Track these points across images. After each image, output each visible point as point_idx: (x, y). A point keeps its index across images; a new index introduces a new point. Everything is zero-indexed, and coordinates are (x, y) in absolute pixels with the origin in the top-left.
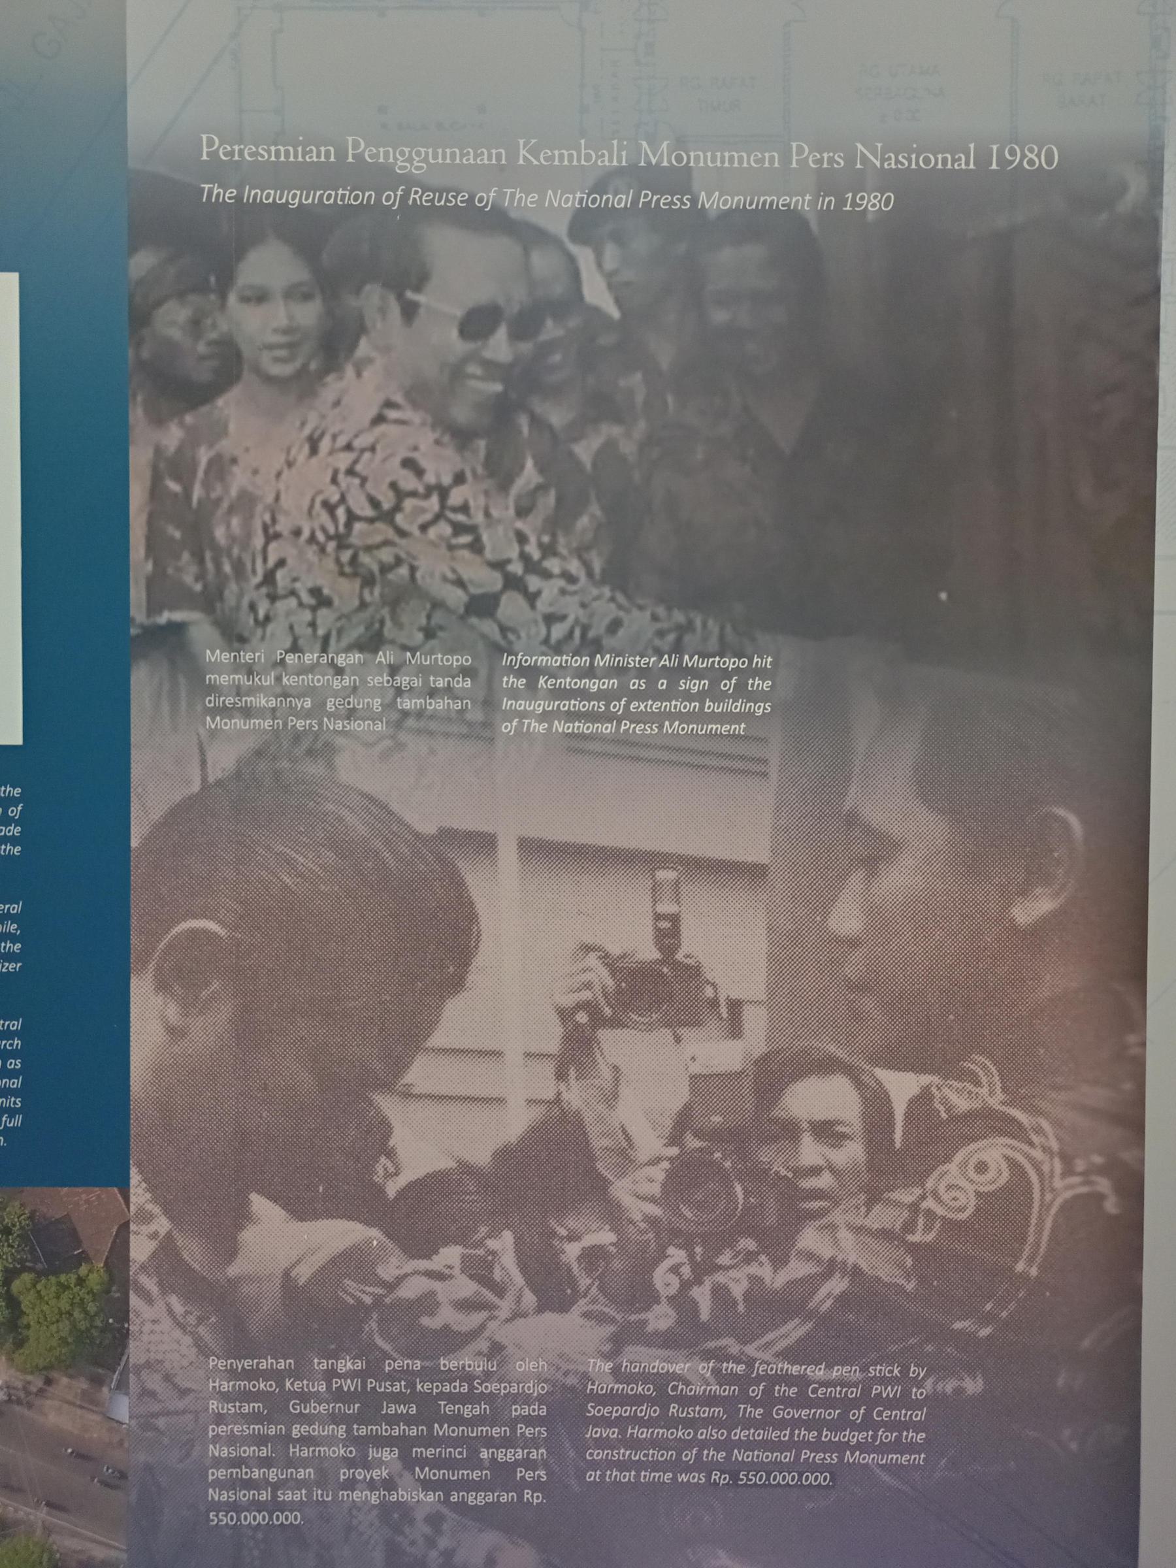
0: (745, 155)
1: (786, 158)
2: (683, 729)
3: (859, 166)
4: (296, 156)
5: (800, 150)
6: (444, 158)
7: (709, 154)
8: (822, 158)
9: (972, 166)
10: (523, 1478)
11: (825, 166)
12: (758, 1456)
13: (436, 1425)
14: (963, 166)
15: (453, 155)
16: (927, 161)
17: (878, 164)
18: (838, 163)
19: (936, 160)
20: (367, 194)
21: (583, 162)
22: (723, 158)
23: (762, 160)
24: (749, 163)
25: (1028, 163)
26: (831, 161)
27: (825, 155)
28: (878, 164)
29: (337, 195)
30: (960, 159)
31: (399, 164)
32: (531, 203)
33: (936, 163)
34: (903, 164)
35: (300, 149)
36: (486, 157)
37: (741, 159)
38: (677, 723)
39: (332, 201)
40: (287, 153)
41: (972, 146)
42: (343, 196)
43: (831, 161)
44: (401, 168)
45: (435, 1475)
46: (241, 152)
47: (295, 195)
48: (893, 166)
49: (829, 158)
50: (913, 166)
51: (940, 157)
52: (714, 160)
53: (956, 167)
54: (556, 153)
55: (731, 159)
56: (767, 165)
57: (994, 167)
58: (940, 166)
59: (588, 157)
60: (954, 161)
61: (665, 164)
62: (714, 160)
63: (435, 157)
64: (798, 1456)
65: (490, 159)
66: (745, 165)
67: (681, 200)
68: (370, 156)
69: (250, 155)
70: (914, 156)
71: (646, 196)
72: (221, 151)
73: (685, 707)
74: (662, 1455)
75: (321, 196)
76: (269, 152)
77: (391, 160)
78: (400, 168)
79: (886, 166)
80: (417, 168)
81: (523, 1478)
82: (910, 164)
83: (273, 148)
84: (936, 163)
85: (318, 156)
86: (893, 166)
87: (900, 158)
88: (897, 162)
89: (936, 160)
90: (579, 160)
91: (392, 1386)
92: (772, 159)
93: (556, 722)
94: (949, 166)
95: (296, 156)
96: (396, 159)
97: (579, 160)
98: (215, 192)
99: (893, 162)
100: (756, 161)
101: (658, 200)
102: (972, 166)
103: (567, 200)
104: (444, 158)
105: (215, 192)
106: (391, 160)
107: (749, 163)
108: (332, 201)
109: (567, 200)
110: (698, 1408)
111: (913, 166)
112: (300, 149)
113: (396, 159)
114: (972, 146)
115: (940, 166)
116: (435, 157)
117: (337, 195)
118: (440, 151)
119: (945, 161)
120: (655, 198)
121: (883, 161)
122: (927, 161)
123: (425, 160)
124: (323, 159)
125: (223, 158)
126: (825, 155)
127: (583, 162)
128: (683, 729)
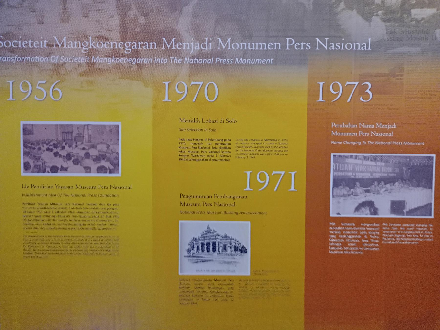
0: (265, 44)
2: (244, 61)
5: (291, 42)
6: (255, 47)
7: (249, 44)
9: (369, 49)
11: (302, 48)
12: (196, 61)
13: (237, 59)
16: (349, 46)
17: (326, 48)
18: (308, 48)
19: (353, 45)
22: (255, 45)
23: (273, 47)
26: (305, 46)
27: (302, 44)
28: (326, 48)
30: (364, 45)
33: (353, 47)
34: (338, 48)
37: (263, 46)
41: (370, 39)
43: (305, 46)
48: (333, 49)
49: (304, 45)
50: (343, 49)
52: (251, 46)
54: (275, 44)
55: (259, 46)
56: (275, 48)
62: (251, 46)
64: (214, 61)
66: (265, 49)
68: (297, 47)
70: (343, 44)
71: (218, 60)
72: (295, 45)
73: (200, 61)
74: (200, 61)
75: (143, 60)
79: (330, 49)
80: (127, 51)
84: (353, 47)
85: (74, 45)
86: (333, 49)
88: (335, 46)
89: (353, 45)
91: (226, 62)
92: (277, 46)
93: (186, 58)
96: (82, 47)
99: (333, 46)
101: (222, 61)
103: (191, 61)
104: (255, 47)
105: (175, 60)
109: (191, 61)
111: (343, 49)
114: (370, 39)
115: (355, 49)
119: (357, 46)
121: (329, 46)
128: (244, 61)
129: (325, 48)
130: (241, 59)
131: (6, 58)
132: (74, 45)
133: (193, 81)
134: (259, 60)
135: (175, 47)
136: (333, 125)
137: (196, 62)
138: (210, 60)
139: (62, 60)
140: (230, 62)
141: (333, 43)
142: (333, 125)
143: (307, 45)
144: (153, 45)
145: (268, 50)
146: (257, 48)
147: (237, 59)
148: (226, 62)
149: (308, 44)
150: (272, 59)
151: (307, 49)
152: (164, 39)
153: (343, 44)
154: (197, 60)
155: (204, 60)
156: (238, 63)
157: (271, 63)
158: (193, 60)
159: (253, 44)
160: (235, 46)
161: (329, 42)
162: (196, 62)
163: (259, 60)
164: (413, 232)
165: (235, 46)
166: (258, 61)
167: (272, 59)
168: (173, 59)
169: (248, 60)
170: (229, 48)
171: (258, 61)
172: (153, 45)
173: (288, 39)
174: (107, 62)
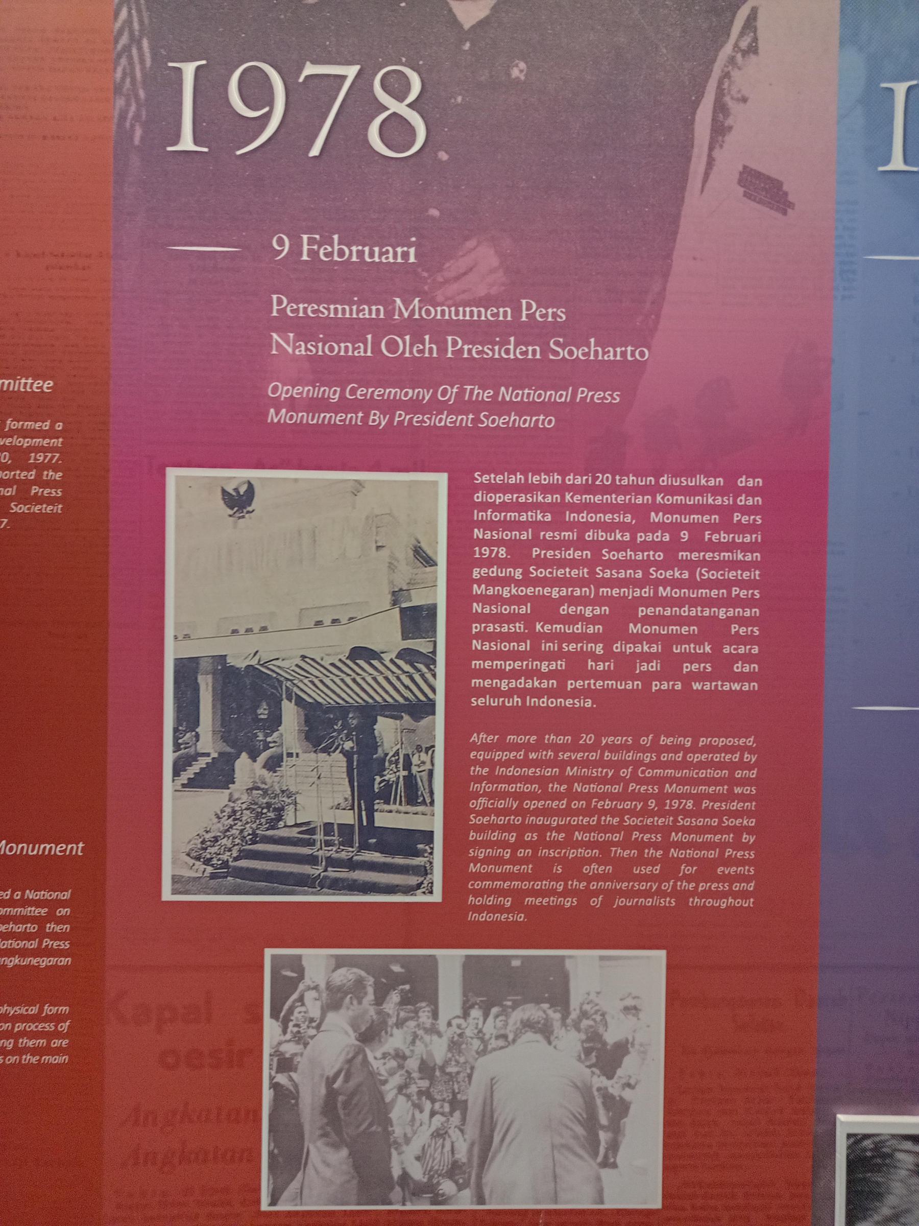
4: (351, 314)
6: (464, 315)
8: (498, 313)
9: (369, 354)
10: (737, 632)
11: (550, 319)
16: (331, 349)
18: (561, 318)
20: (548, 393)
23: (497, 315)
24: (486, 317)
28: (290, 350)
29: (523, 394)
30: (359, 347)
32: (488, 397)
34: (311, 351)
35: (354, 308)
39: (519, 399)
40: (344, 310)
42: (529, 394)
43: (555, 315)
45: (646, 630)
46: (305, 309)
47: (525, 420)
48: (303, 353)
49: (553, 313)
50: (320, 353)
51: (342, 345)
52: (457, 314)
53: (297, 353)
55: (472, 312)
58: (342, 353)
61: (417, 316)
62: (457, 314)
67: (611, 395)
69: (313, 312)
70: (497, 348)
71: (583, 392)
72: (289, 309)
73: (539, 396)
76: (328, 309)
81: (737, 632)
82: (317, 352)
83: (332, 307)
84: (339, 351)
86: (303, 353)
88: (307, 349)
92: (505, 312)
93: (503, 389)
94: (350, 354)
95: (351, 314)
98: (476, 392)
99: (303, 348)
100: (492, 315)
101: (593, 396)
102: (369, 354)
104: (464, 315)
105: (476, 392)
108: (519, 399)
110: (656, 819)
111: (497, 356)
112: (354, 308)
117: (523, 394)
120: (590, 394)
122: (331, 349)
125: (540, 319)
126: (550, 311)
129: (287, 351)
131: (528, 418)
135: (420, 314)
136: (279, 304)
137: (25, 387)
138: (564, 393)
139: (483, 422)
141: (302, 344)
142: (279, 304)
143: (559, 313)
144: (378, 310)
146: (468, 318)
149: (562, 312)
151: (559, 320)
152: (398, 301)
154: (532, 392)
155: (548, 393)
157: (80, 854)
158: (520, 392)
160: (428, 312)
161: (295, 342)
162: (25, 387)
168: (472, 391)
169: (416, 391)
172: (378, 310)
174: (329, 397)
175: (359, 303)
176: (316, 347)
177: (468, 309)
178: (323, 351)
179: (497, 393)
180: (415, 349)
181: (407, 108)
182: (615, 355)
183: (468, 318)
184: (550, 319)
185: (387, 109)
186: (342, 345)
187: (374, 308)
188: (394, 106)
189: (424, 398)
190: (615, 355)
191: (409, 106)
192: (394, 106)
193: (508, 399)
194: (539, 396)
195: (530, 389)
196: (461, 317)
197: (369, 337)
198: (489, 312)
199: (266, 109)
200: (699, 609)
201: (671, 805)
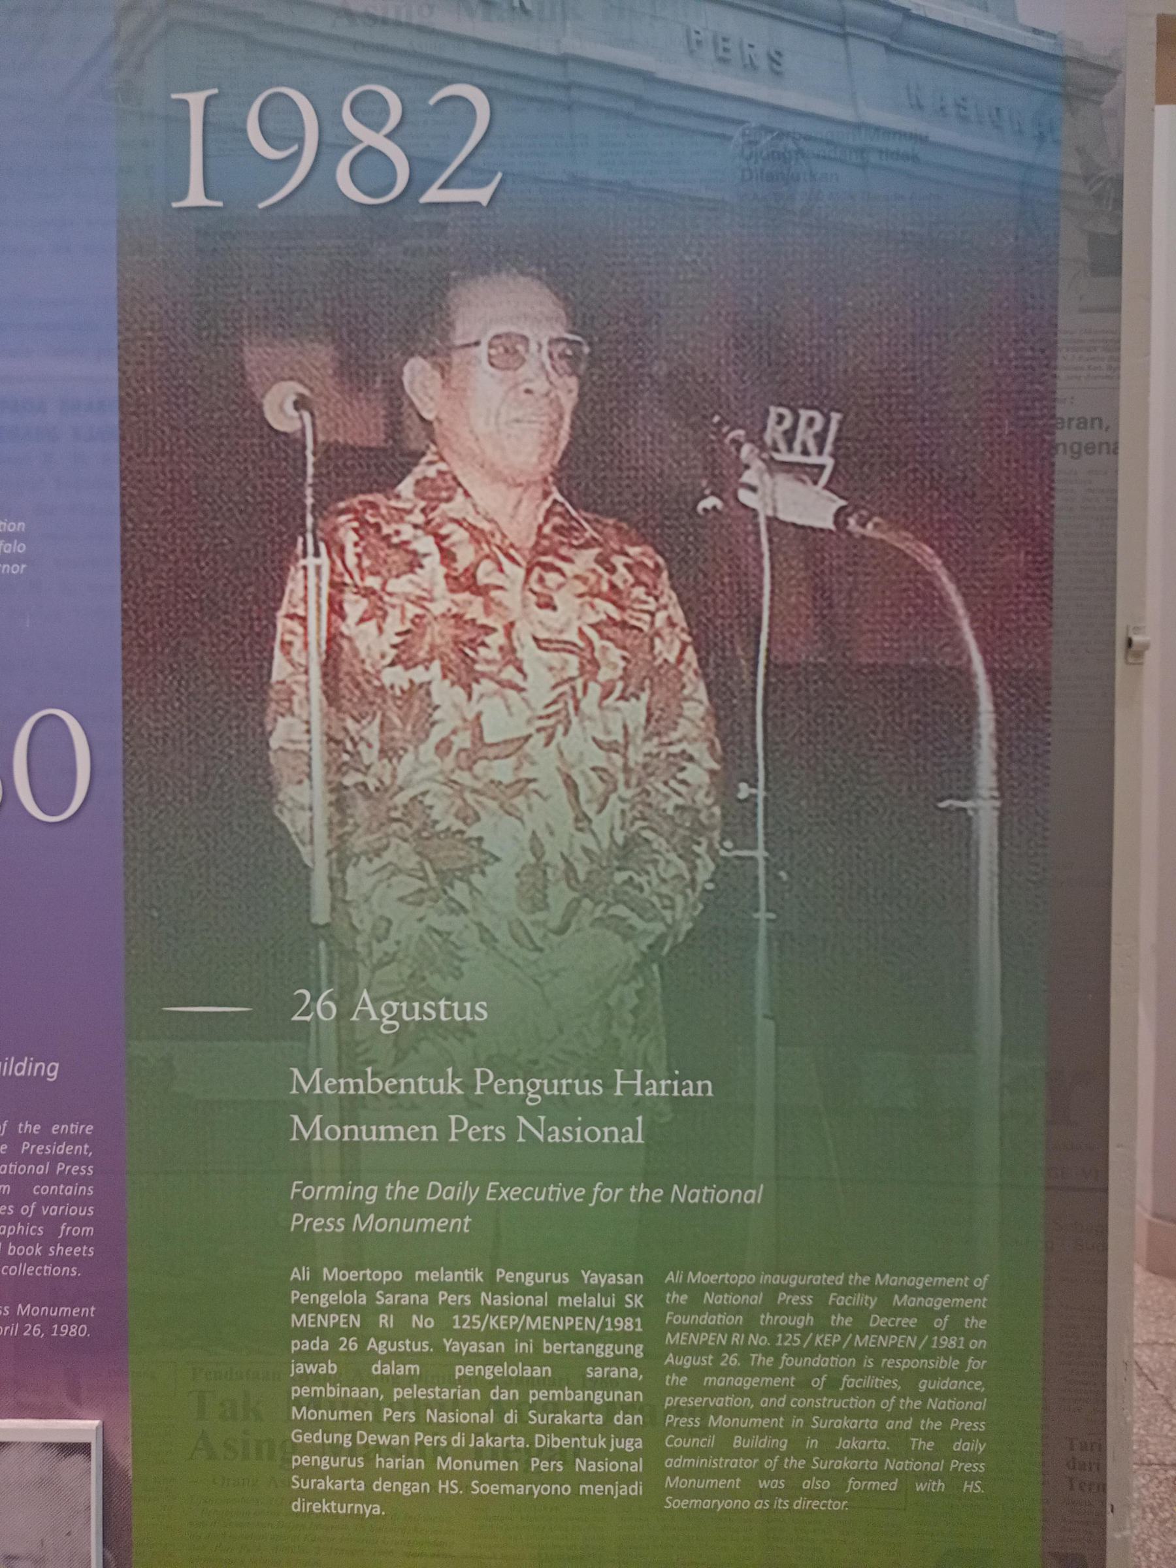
0: (401, 1129)
1: (444, 1132)
3: (521, 1140)
5: (459, 1124)
6: (378, 1135)
7: (364, 1128)
9: (640, 1140)
11: (486, 1139)
14: (655, 1093)
15: (611, 1134)
16: (593, 1135)
18: (481, 1016)
21: (370, 1091)
23: (420, 1134)
25: (386, 111)
28: (541, 1137)
31: (385, 1022)
33: (342, 1136)
34: (429, 1015)
36: (691, 1089)
38: (372, 1216)
42: (709, 1195)
43: (492, 1134)
44: (532, 1100)
50: (579, 1140)
51: (606, 1130)
52: (369, 1134)
54: (424, 1128)
55: (387, 1132)
57: (640, 1119)
58: (606, 1140)
59: (375, 1086)
60: (680, 1089)
62: (369, 1134)
63: (551, 1088)
65: (695, 1090)
70: (578, 1129)
71: (298, 1219)
72: (470, 1132)
73: (722, 1196)
77: (522, 1092)
78: (386, 1027)
84: (342, 1136)
85: (695, 1090)
87: (477, 1008)
88: (561, 1135)
90: (366, 1089)
91: (325, 1226)
92: (430, 1132)
94: (616, 1140)
96: (526, 1090)
97: (366, 1089)
99: (557, 1135)
100: (413, 1135)
101: (311, 1224)
102: (640, 1140)
104: (378, 1135)
106: (522, 1092)
107: (322, 1088)
111: (579, 1140)
113: (526, 1090)
115: (606, 1140)
116: (551, 1088)
118: (374, 1128)
121: (547, 1134)
122: (593, 1135)
123: (541, 1092)
124: (700, 1094)
126: (486, 1128)
127: (370, 1091)
128: (381, 1225)
130: (372, 1216)
132: (695, 1090)
133: (477, 204)
134: (427, 1222)
135: (322, 1135)
137: (708, 1197)
140: (336, 1226)
144: (705, 1087)
145: (407, 1142)
147: (358, 1216)
148: (325, 1226)
150: (467, 1220)
153: (578, 1129)
156: (362, 1229)
159: (374, 1128)
160: (333, 1133)
162: (708, 1197)
163: (427, 1222)
164: (541, 1323)
165: (333, 1133)
166: (422, 1224)
167: (467, 1220)
170: (318, 1138)
171: (422, 1224)
172: (705, 1087)
173: (453, 1118)
175: (680, 1079)
176: (574, 1133)
177: (382, 1128)
178: (582, 1137)
179: (668, 1192)
180: (326, 1085)
181: (387, 141)
182: (659, 1090)
183: (382, 1139)
184: (486, 1139)
185: (361, 142)
186: (606, 1130)
187: (700, 1083)
188: (368, 137)
189: (468, 1199)
190: (659, 1090)
191: (389, 136)
192: (368, 137)
193: (682, 1200)
194: (722, 1196)
195: (710, 1187)
196: (374, 1138)
197: (640, 1119)
198: (409, 1132)
199: (295, 148)
200: (437, 1389)
201: (59, 1332)
